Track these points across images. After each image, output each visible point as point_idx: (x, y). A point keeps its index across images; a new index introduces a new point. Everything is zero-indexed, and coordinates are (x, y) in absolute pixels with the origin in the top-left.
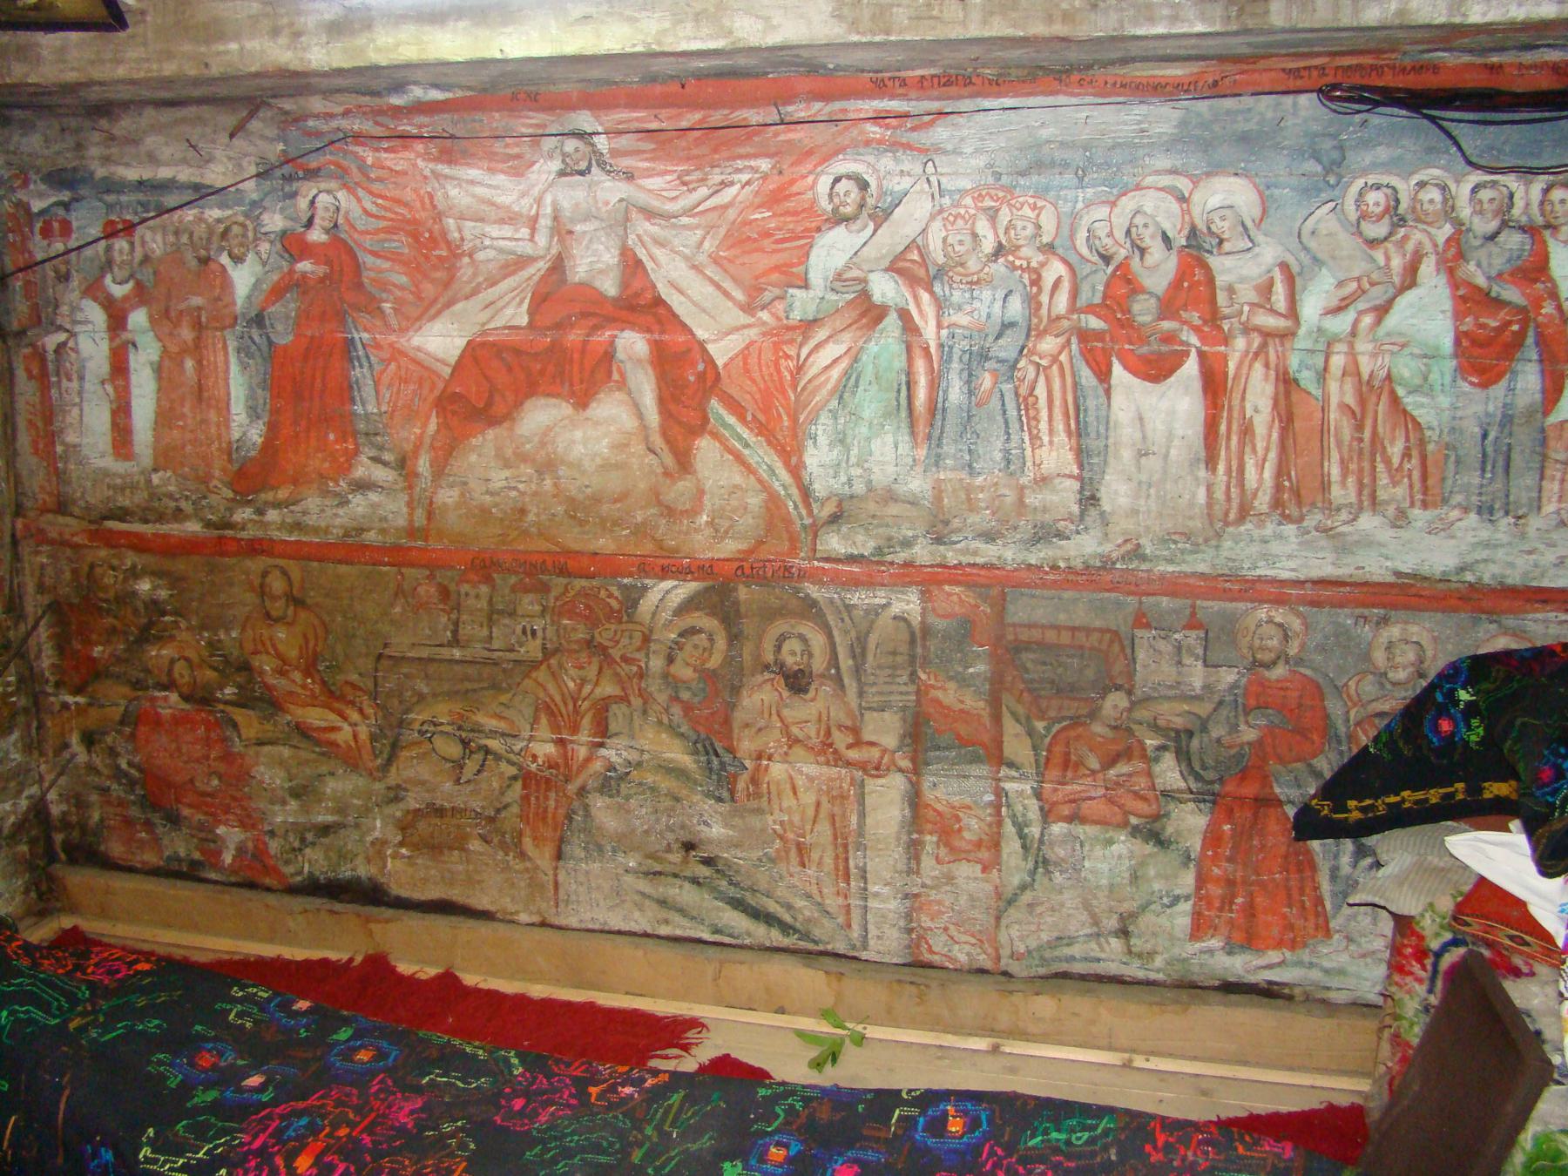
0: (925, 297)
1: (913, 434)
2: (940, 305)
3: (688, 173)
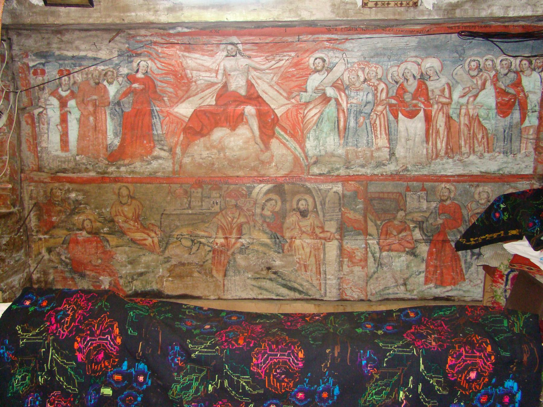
0: (343, 94)
1: (339, 136)
2: (347, 97)
3: (268, 56)
